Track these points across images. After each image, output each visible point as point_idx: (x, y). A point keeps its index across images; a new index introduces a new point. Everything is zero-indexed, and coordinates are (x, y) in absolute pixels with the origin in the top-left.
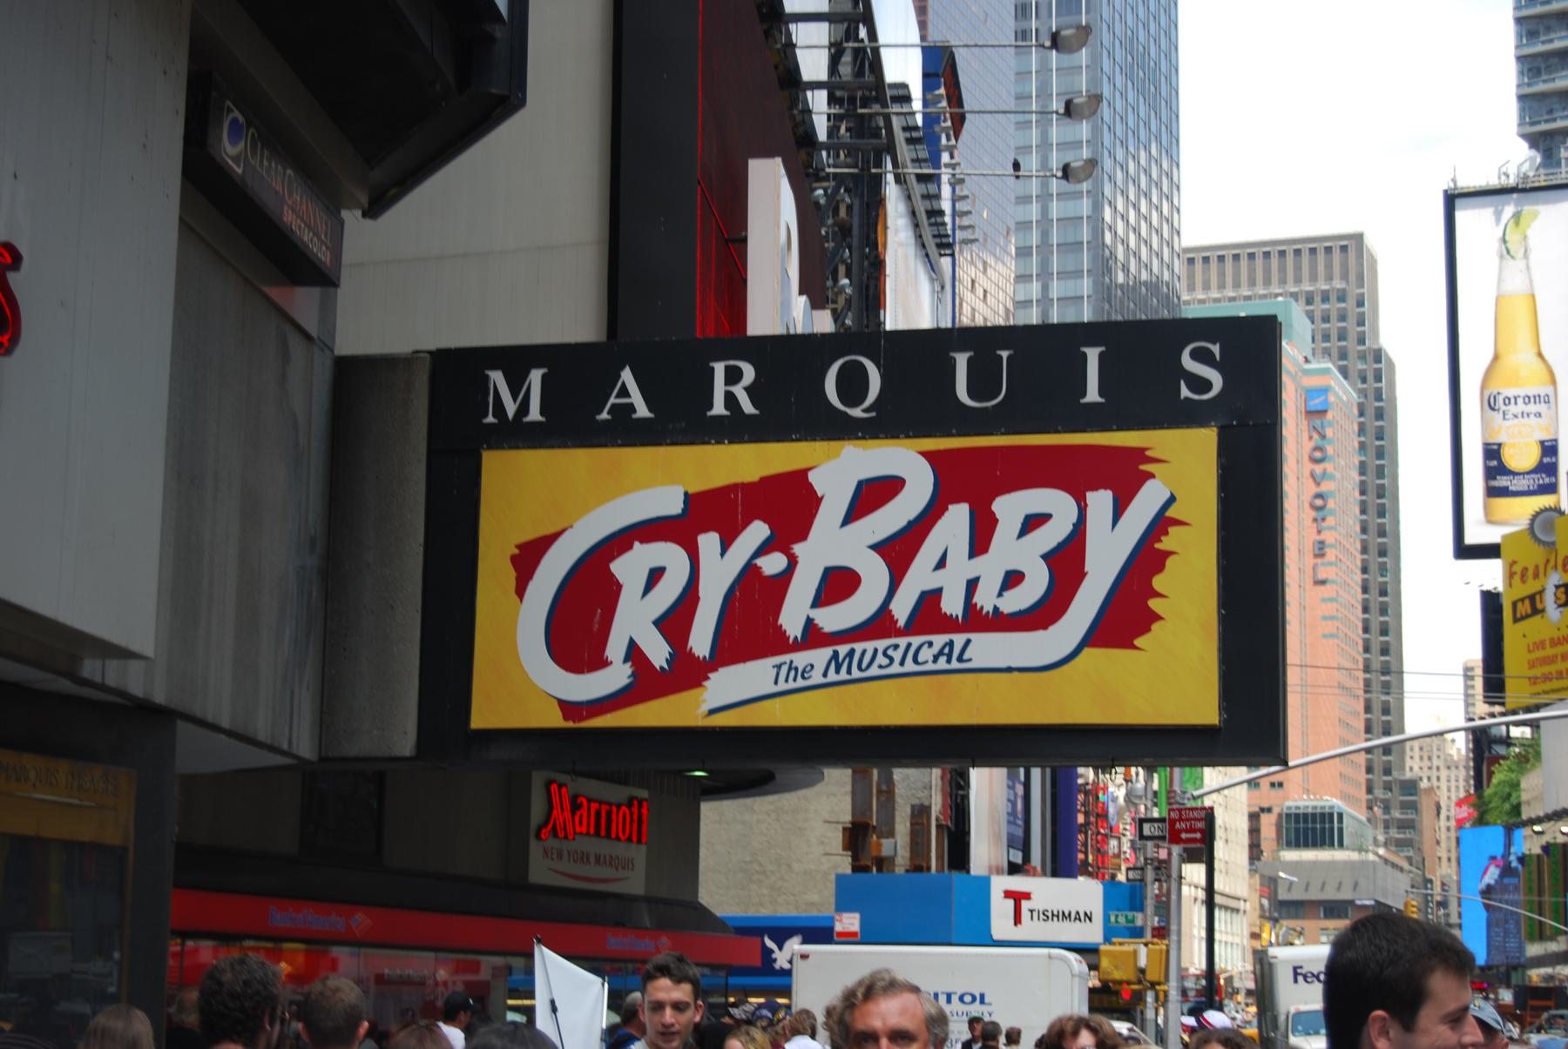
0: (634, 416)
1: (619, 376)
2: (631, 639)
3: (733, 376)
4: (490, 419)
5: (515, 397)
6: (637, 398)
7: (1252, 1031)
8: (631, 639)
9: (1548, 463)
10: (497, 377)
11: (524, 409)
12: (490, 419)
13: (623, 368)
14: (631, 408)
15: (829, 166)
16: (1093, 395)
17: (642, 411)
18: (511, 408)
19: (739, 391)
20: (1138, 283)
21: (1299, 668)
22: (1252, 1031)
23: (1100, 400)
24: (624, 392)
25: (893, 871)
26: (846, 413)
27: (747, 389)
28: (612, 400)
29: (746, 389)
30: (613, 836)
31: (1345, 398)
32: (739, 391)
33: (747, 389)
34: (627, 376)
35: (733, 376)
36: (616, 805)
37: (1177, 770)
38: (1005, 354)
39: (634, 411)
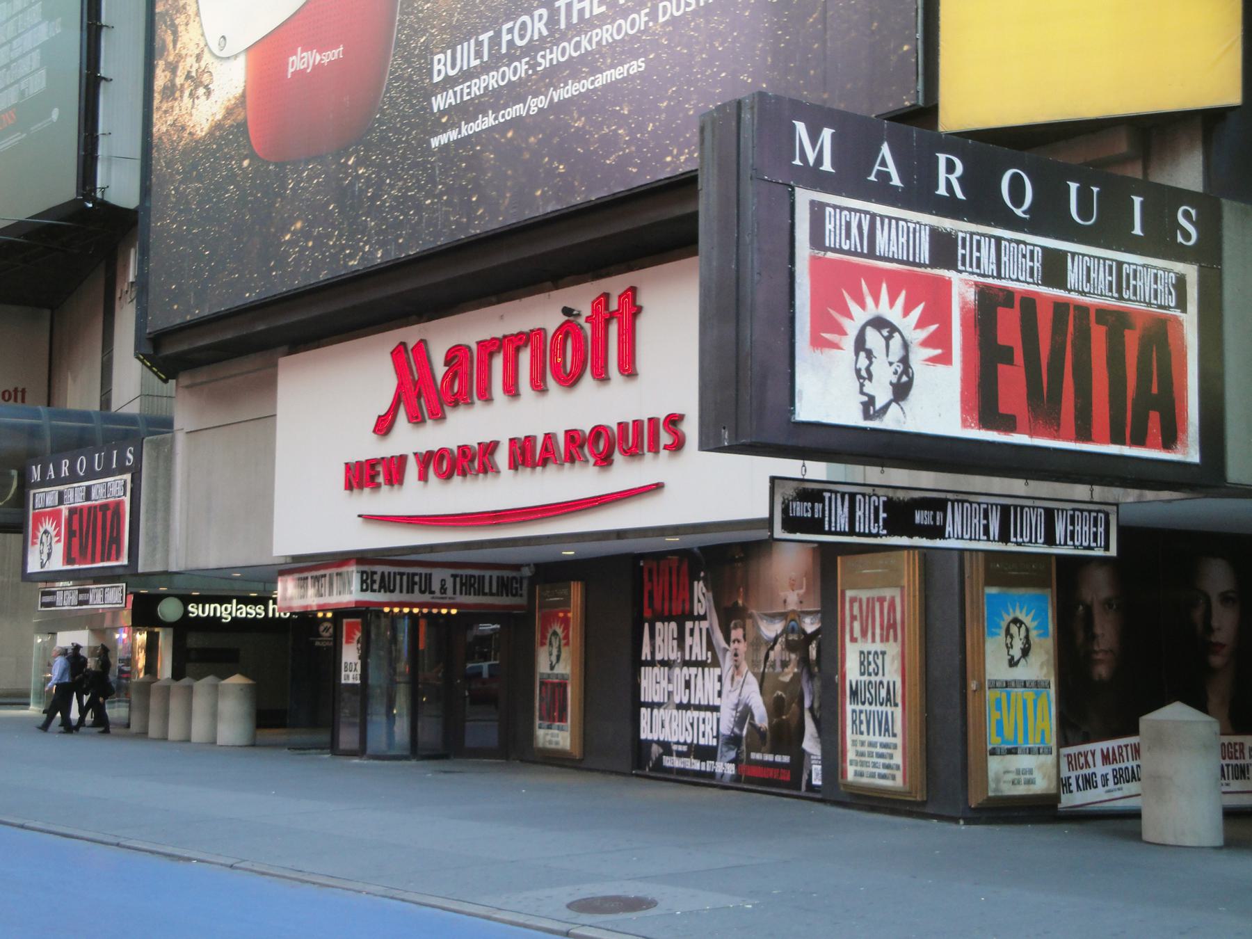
4: (797, 162)
5: (814, 147)
6: (892, 169)
7: (436, 79)
9: (782, 753)
11: (819, 160)
12: (797, 162)
13: (881, 144)
14: (887, 176)
16: (1138, 231)
17: (896, 181)
18: (811, 157)
22: (436, 79)
23: (1141, 234)
24: (883, 163)
27: (959, 179)
28: (877, 167)
29: (958, 179)
30: (847, 497)
31: (1155, 390)
32: (953, 178)
34: (885, 150)
35: (951, 168)
37: (496, 723)
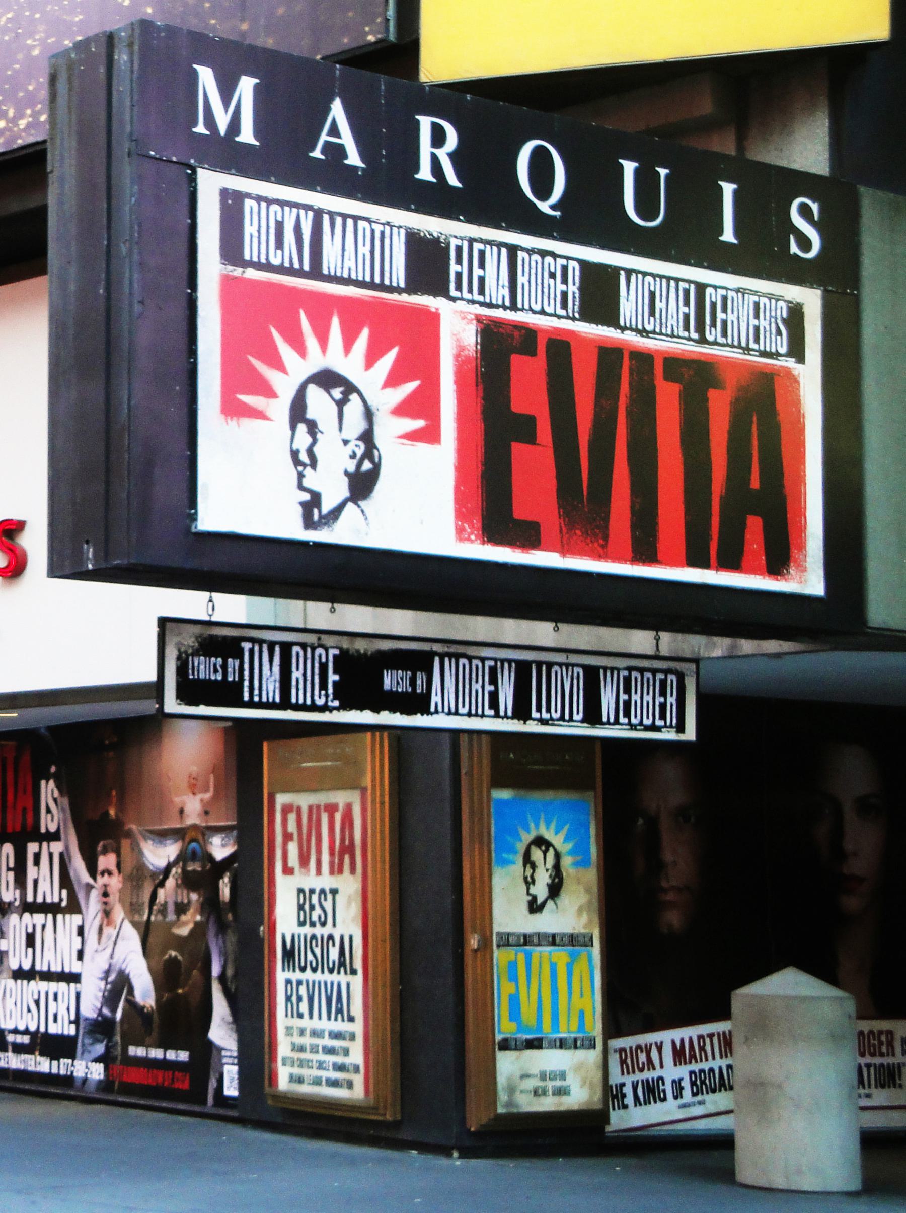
0: (346, 162)
1: (327, 110)
2: (315, 470)
3: (438, 138)
5: (226, 102)
6: (347, 139)
8: (315, 470)
10: (206, 76)
13: (331, 100)
15: (14, 121)
17: (354, 158)
18: (223, 122)
19: (442, 154)
20: (205, 656)
21: (547, 1030)
24: (334, 131)
25: (498, 782)
26: (534, 204)
27: (451, 155)
33: (451, 155)
34: (337, 110)
35: (438, 138)
36: (310, 647)
38: (663, 172)
39: (345, 156)
